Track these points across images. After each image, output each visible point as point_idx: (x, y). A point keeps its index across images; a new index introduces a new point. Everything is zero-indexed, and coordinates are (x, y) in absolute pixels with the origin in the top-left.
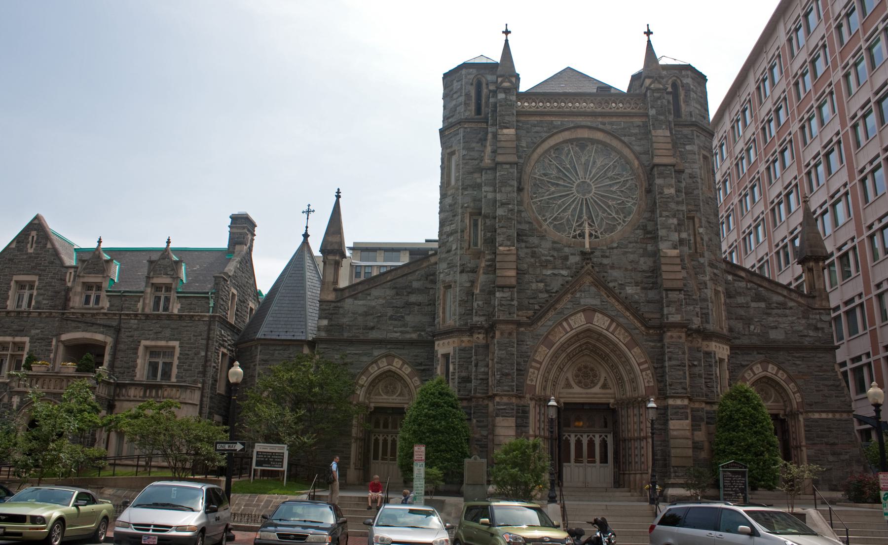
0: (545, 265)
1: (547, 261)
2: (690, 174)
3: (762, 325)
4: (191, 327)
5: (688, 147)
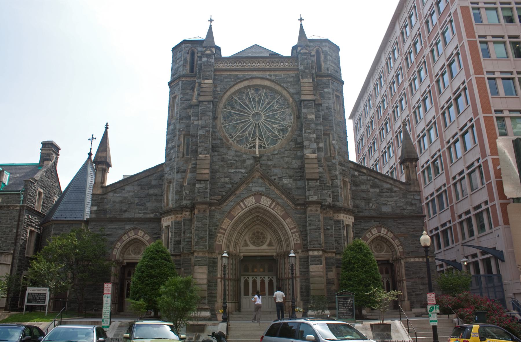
0: (230, 166)
1: (231, 164)
2: (327, 107)
3: (377, 203)
4: (8, 213)
5: (326, 90)
